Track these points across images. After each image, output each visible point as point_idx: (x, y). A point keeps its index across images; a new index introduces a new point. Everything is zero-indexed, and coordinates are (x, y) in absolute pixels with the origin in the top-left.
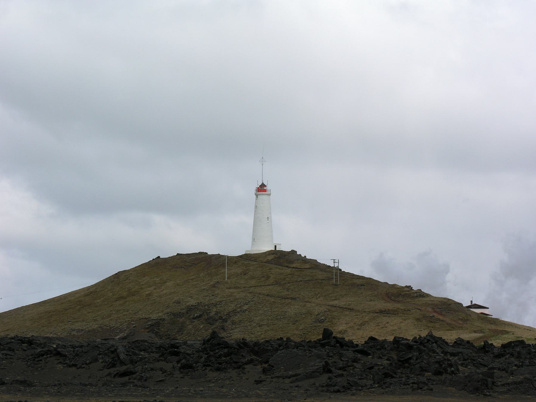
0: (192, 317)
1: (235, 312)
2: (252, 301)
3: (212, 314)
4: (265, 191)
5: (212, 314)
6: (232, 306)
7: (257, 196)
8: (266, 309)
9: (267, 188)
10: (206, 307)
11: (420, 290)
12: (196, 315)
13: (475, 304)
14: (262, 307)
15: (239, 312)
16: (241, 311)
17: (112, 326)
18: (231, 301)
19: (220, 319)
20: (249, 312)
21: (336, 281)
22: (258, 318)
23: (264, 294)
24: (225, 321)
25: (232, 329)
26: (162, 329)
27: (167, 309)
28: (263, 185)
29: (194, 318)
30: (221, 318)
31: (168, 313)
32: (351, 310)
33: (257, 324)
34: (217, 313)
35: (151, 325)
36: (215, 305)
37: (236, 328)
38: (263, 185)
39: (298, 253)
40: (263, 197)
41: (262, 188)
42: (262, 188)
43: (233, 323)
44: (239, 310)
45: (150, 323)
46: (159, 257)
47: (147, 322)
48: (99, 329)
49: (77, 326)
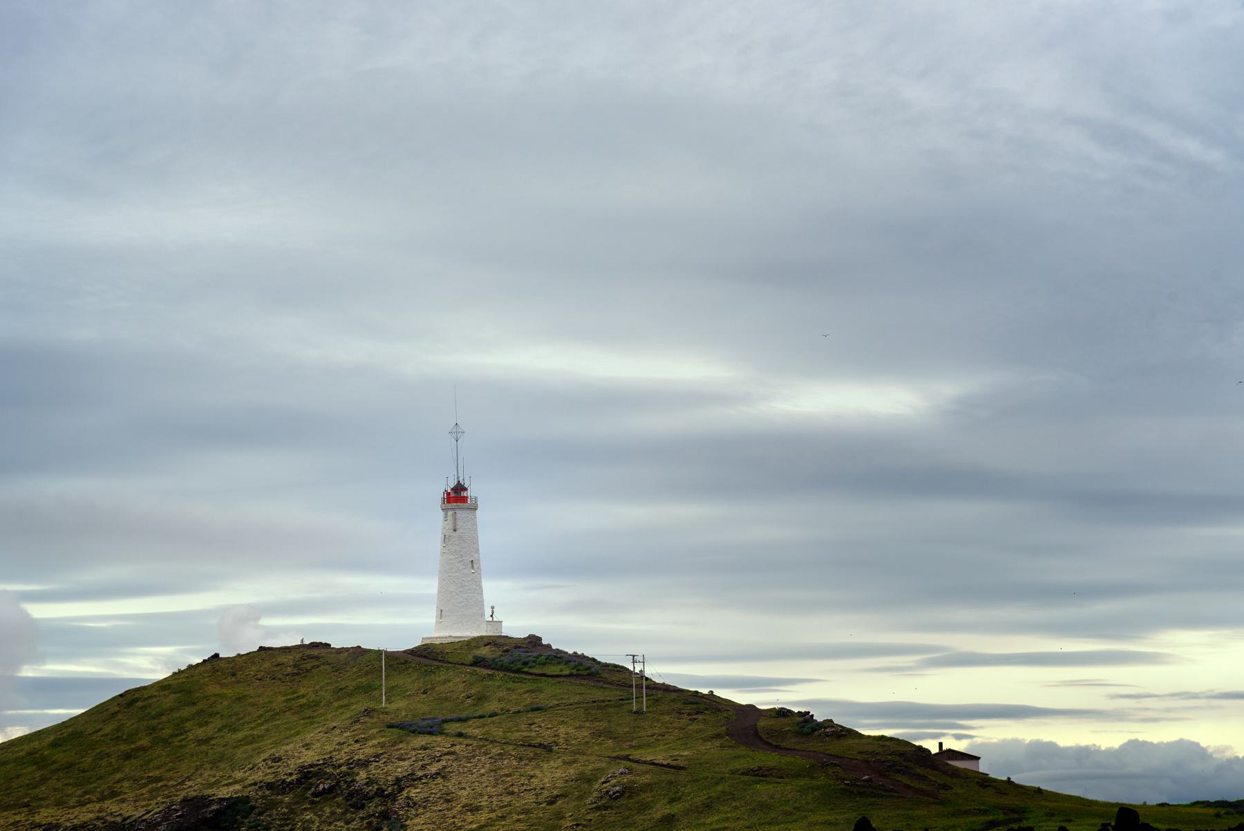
1: (412, 779)
10: (344, 768)
11: (831, 721)
12: (321, 787)
13: (950, 751)
15: (420, 779)
17: (127, 815)
24: (393, 797)
28: (460, 488)
30: (380, 793)
31: (255, 784)
32: (538, 709)
34: (370, 782)
36: (365, 764)
37: (417, 815)
38: (460, 488)
39: (544, 642)
41: (457, 496)
42: (457, 496)
43: (411, 804)
44: (420, 774)
46: (216, 655)
48: (99, 823)
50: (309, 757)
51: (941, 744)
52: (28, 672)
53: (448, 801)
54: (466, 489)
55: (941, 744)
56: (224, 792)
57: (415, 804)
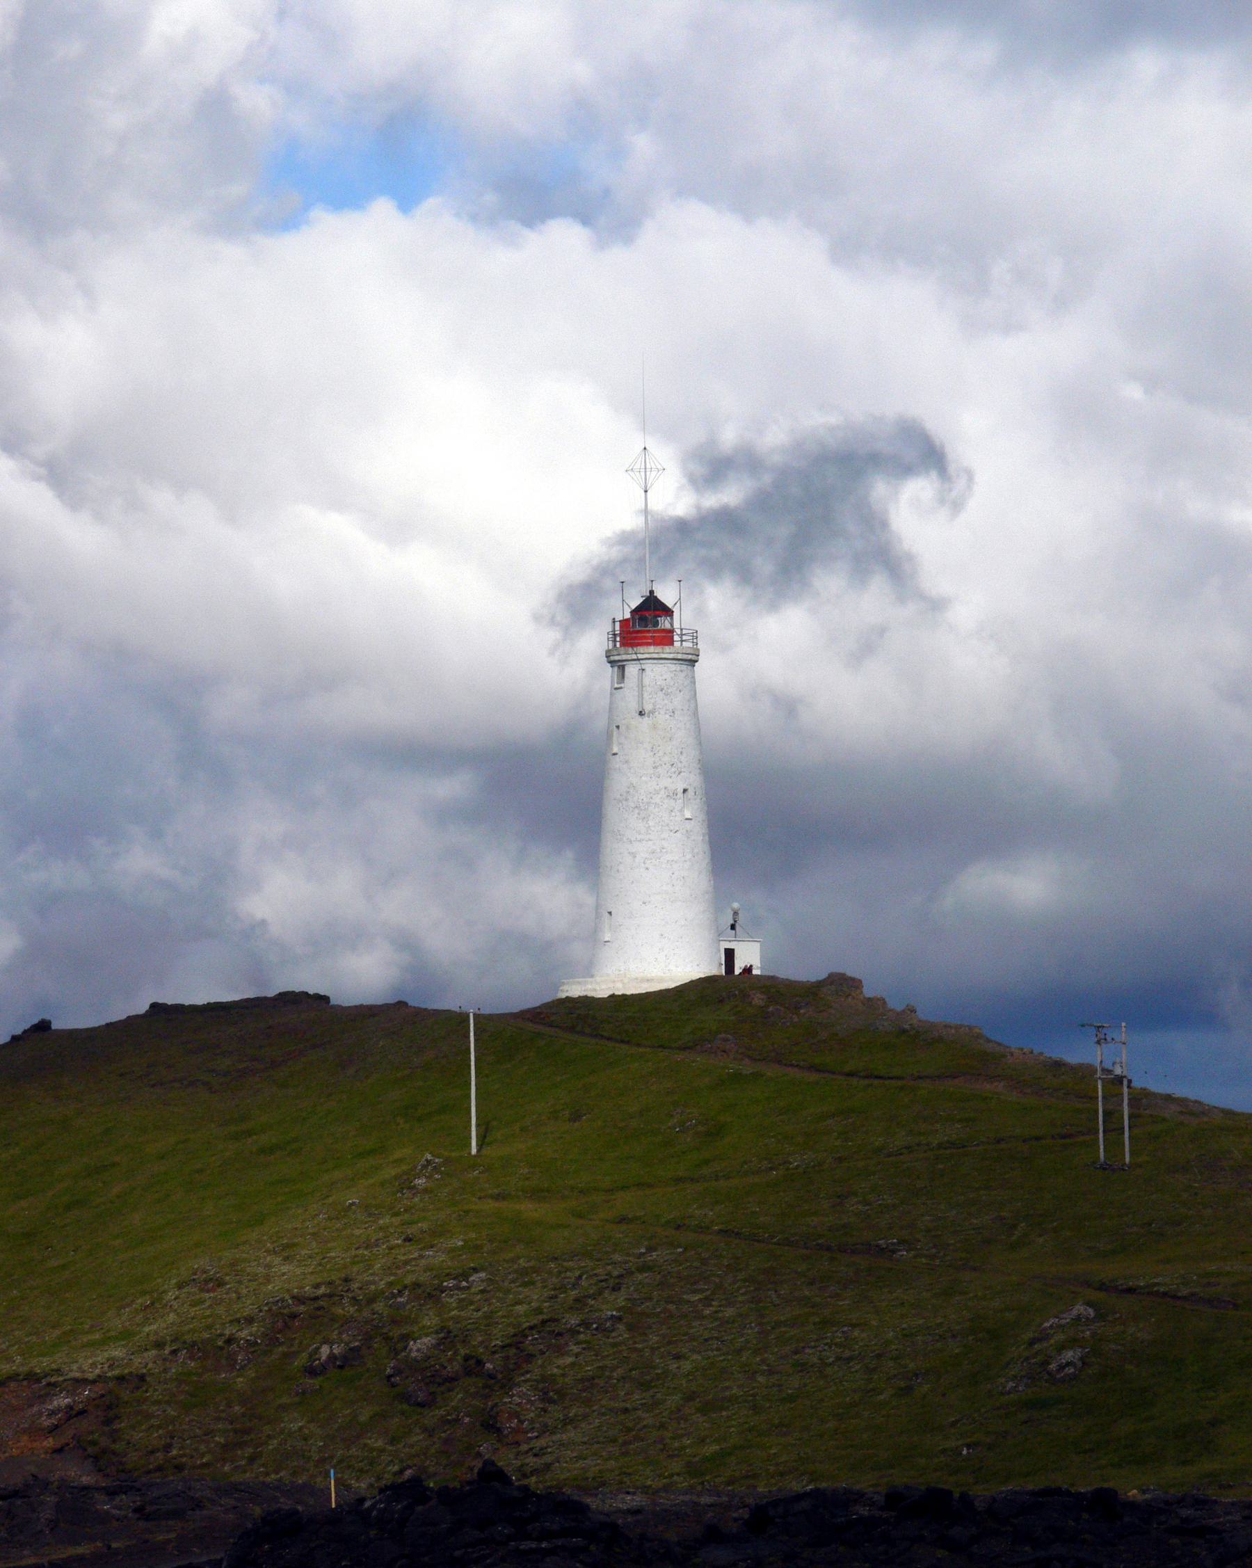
0: (301, 1361)
1: (550, 1330)
2: (643, 1268)
3: (419, 1346)
4: (666, 638)
5: (419, 1346)
6: (528, 1303)
7: (619, 666)
8: (729, 1312)
9: (682, 620)
12: (325, 1351)
14: (707, 1301)
15: (573, 1332)
16: (585, 1324)
18: (523, 1272)
19: (468, 1373)
20: (630, 1328)
21: (1114, 1144)
22: (687, 1366)
23: (702, 1229)
25: (545, 1430)
26: (137, 1436)
27: (146, 1321)
28: (652, 609)
29: (311, 1372)
30: (473, 1365)
31: (159, 1345)
33: (690, 1397)
34: (447, 1338)
35: (73, 1414)
36: (431, 1295)
37: (568, 1422)
38: (652, 609)
40: (654, 671)
43: (550, 1393)
44: (573, 1320)
45: (62, 1401)
47: (42, 1398)
49: (824, 1485)
50: (289, 1277)
51: (730, 954)
52: (474, 1151)
53: (644, 1386)
54: (668, 612)
55: (730, 954)
56: (88, 1364)
57: (562, 1394)
